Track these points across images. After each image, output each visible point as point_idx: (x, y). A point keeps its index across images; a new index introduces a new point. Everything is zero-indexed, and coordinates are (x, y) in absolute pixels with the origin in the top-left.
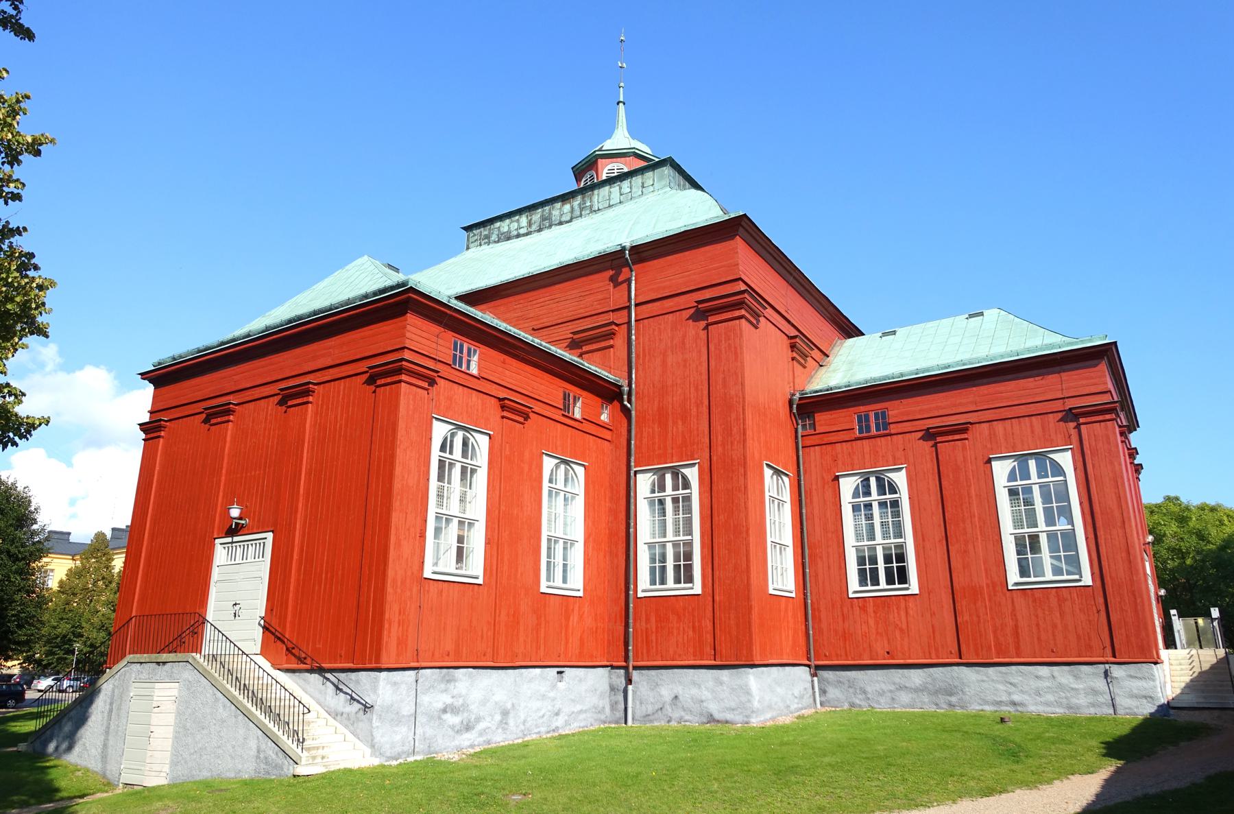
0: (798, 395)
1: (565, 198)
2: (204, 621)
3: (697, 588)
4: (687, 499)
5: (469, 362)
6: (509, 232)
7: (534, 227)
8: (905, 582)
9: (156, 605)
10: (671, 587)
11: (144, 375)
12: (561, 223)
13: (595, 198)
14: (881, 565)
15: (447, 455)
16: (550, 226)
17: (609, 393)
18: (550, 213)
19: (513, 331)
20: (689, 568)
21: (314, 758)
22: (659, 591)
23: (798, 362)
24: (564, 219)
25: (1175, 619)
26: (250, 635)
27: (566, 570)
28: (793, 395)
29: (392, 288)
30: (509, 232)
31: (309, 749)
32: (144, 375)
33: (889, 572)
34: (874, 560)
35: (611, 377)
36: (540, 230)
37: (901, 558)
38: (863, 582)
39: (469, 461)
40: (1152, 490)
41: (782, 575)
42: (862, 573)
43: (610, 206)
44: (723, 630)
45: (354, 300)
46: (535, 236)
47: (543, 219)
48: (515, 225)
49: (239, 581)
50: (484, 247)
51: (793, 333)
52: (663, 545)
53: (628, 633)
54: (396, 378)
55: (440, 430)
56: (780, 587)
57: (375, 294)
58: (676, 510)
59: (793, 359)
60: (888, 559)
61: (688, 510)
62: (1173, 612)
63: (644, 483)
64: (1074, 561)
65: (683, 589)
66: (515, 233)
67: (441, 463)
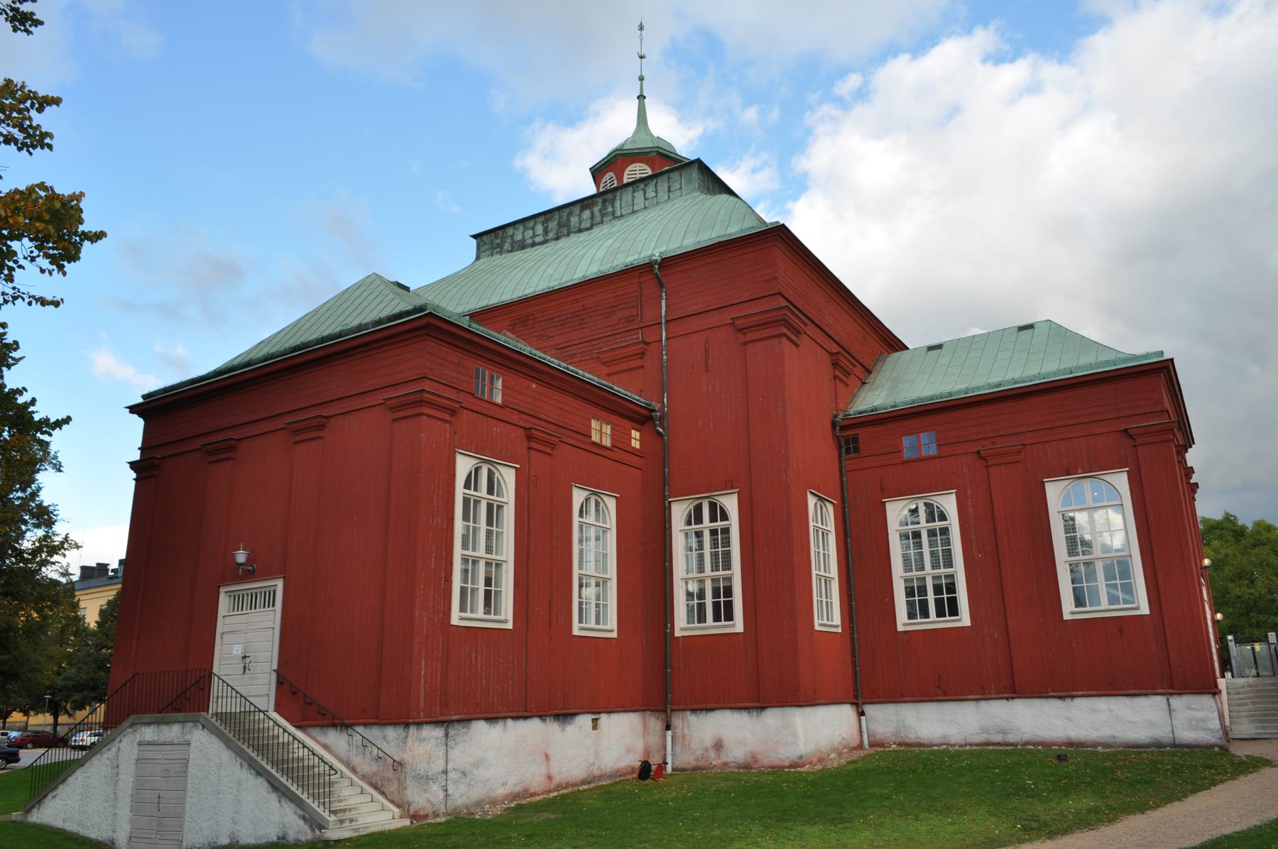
0: (841, 416)
1: (585, 203)
2: (209, 675)
3: (738, 625)
4: (726, 531)
5: (491, 389)
6: (523, 240)
7: (551, 235)
8: (957, 614)
9: (141, 655)
10: (711, 627)
11: (133, 409)
12: (580, 231)
13: (617, 204)
14: (931, 597)
15: (472, 492)
16: (568, 234)
17: (643, 418)
18: (568, 220)
19: (539, 354)
20: (729, 605)
21: (341, 821)
22: (697, 630)
23: (841, 380)
24: (583, 226)
25: (1232, 645)
26: (260, 688)
27: (596, 610)
28: (836, 416)
29: (408, 313)
30: (523, 240)
31: (335, 812)
32: (133, 409)
33: (939, 603)
34: (923, 590)
35: (642, 401)
36: (557, 238)
37: (951, 588)
38: (911, 615)
39: (494, 498)
40: (1207, 508)
41: (828, 613)
42: (910, 605)
43: (634, 212)
44: (765, 671)
45: (366, 326)
46: (552, 244)
47: (560, 226)
48: (529, 233)
49: (247, 639)
50: (496, 257)
51: (835, 348)
52: (701, 581)
53: (661, 675)
54: (417, 411)
55: (464, 465)
56: (825, 622)
57: (390, 319)
58: (714, 544)
59: (835, 377)
60: (938, 589)
61: (727, 542)
62: (1230, 637)
63: (679, 511)
64: (1128, 589)
65: (723, 628)
66: (530, 241)
67: (466, 501)
